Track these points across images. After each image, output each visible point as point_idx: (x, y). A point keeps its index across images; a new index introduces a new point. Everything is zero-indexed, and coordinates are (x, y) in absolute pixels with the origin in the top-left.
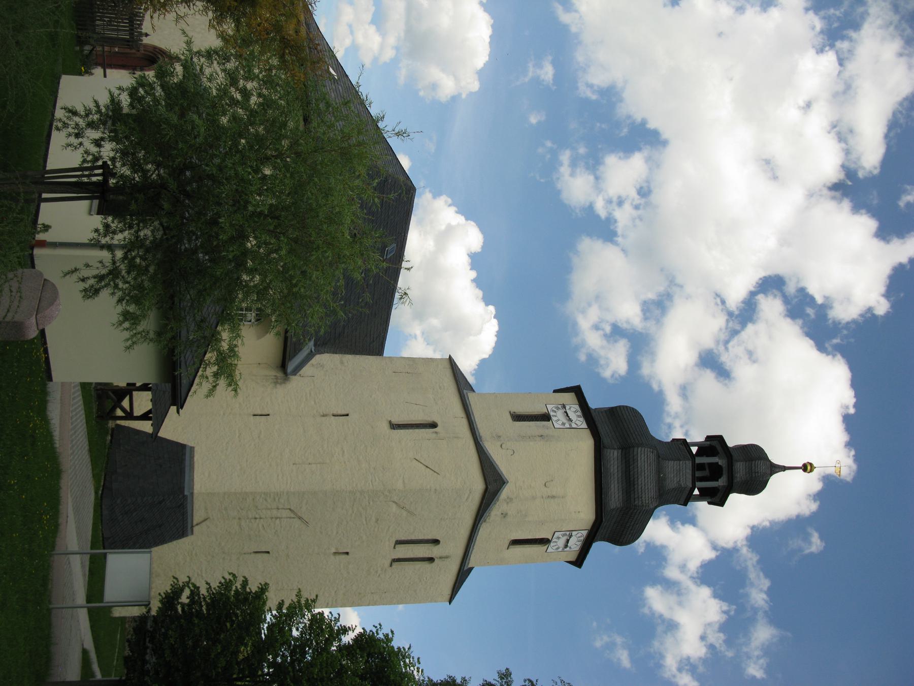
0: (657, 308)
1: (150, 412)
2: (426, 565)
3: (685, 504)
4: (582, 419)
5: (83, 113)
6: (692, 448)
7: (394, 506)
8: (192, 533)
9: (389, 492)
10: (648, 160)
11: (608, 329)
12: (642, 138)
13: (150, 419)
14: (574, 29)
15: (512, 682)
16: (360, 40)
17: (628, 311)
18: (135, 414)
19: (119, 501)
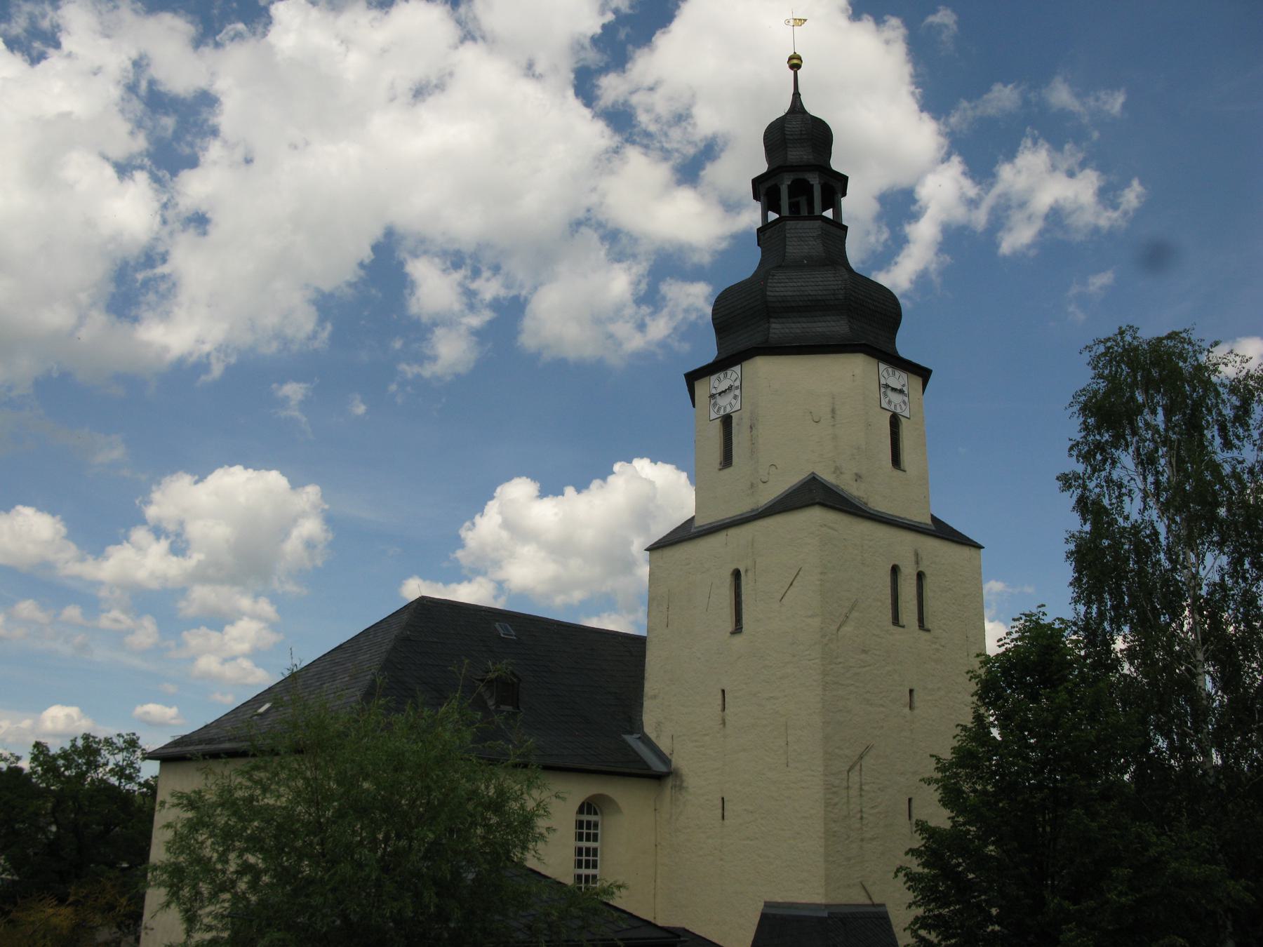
0: (617, 242)
2: (929, 584)
4: (729, 372)
8: (883, 905)
10: (415, 255)
11: (645, 310)
12: (387, 262)
14: (233, 360)
15: (1074, 473)
16: (245, 647)
17: (619, 283)
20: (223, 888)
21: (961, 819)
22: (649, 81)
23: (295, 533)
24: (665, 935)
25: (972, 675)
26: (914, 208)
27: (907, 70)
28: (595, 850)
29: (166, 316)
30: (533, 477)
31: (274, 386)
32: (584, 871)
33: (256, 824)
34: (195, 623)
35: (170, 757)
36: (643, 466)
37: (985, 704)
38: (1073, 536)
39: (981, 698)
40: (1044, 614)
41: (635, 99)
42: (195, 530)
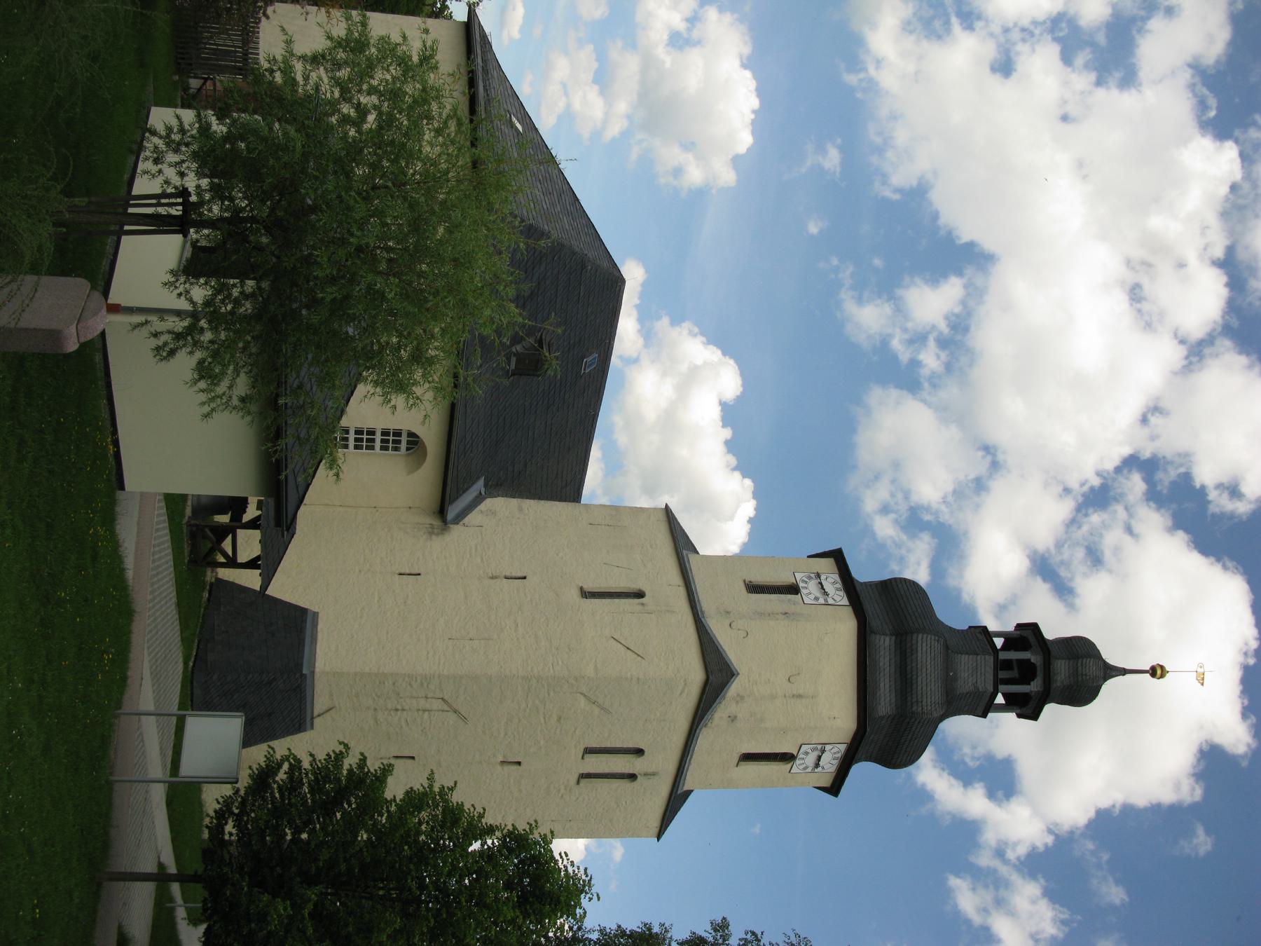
1: (258, 558)
2: (624, 785)
3: (984, 716)
4: (842, 593)
5: (163, 133)
6: (995, 640)
7: (582, 699)
8: (312, 728)
9: (576, 679)
10: (965, 287)
12: (959, 258)
13: (258, 567)
15: (730, 935)
16: (577, 105)
17: (931, 488)
18: (239, 561)
19: (215, 677)
20: (344, 91)
21: (393, 808)
22: (1138, 527)
23: (690, 157)
24: (290, 516)
25: (533, 826)
26: (1000, 794)
27: (1141, 801)
28: (372, 448)
29: (907, 27)
30: (739, 399)
31: (839, 141)
32: (352, 436)
33: (405, 123)
34: (601, 56)
35: (471, 34)
36: (748, 508)
37: (504, 836)
38: (666, 931)
39: (510, 833)
40: (590, 899)
41: (1121, 512)
42: (695, 58)
